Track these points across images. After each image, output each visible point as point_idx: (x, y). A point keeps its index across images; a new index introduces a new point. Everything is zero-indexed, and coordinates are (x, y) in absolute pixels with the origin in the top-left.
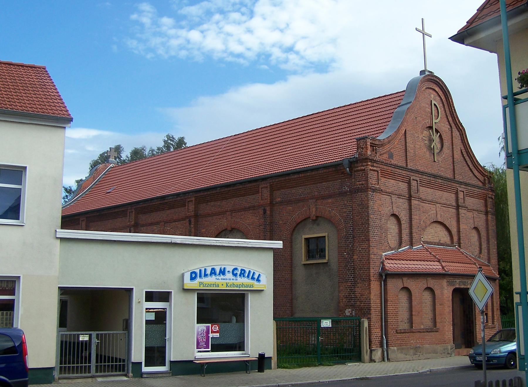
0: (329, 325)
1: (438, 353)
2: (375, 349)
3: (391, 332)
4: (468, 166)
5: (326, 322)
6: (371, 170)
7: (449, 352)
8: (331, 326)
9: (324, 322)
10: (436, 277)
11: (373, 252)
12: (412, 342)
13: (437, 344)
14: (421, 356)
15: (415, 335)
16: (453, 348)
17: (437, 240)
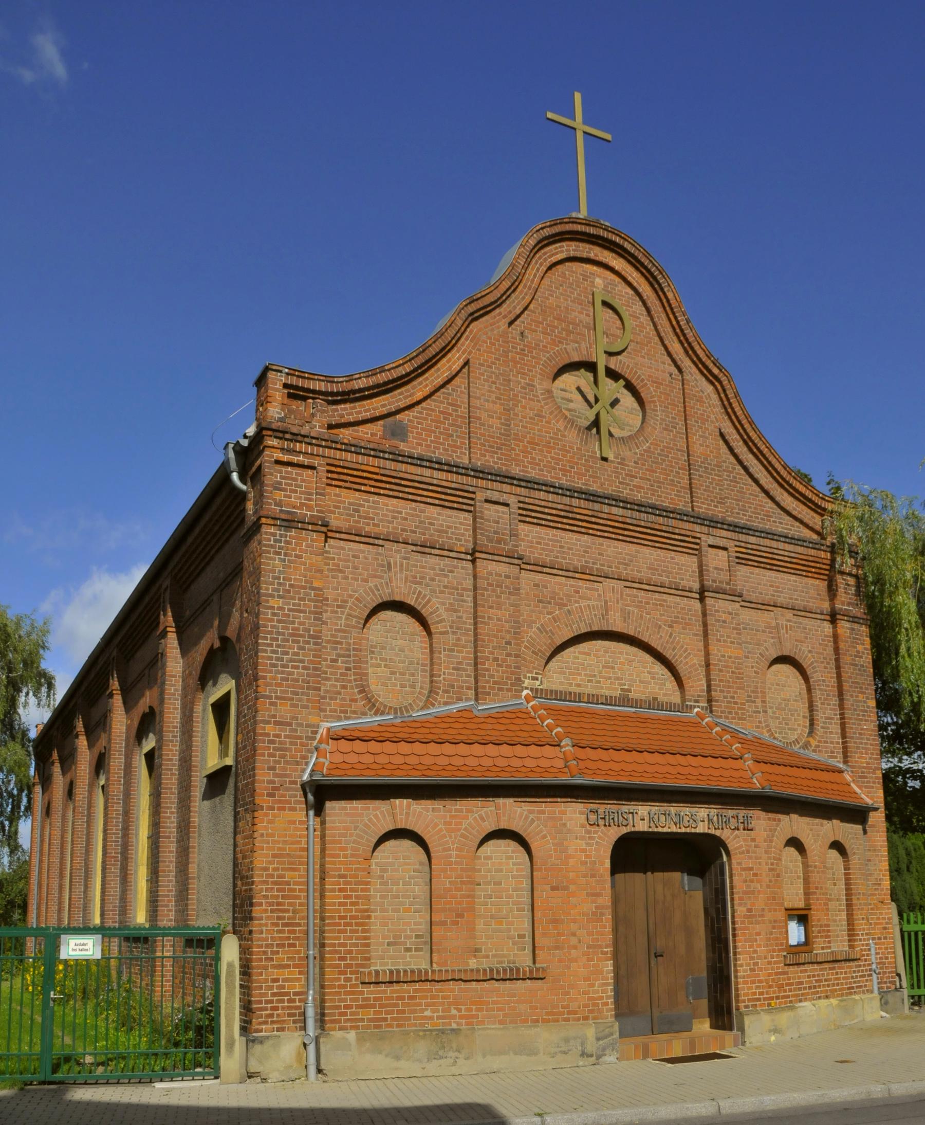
0: (91, 953)
1: (536, 1054)
2: (268, 1037)
3: (339, 979)
4: (756, 481)
5: (78, 941)
6: (278, 462)
7: (590, 1049)
12: (428, 1013)
13: (537, 1021)
14: (461, 1061)
15: (441, 991)
16: (612, 1034)
17: (616, 689)
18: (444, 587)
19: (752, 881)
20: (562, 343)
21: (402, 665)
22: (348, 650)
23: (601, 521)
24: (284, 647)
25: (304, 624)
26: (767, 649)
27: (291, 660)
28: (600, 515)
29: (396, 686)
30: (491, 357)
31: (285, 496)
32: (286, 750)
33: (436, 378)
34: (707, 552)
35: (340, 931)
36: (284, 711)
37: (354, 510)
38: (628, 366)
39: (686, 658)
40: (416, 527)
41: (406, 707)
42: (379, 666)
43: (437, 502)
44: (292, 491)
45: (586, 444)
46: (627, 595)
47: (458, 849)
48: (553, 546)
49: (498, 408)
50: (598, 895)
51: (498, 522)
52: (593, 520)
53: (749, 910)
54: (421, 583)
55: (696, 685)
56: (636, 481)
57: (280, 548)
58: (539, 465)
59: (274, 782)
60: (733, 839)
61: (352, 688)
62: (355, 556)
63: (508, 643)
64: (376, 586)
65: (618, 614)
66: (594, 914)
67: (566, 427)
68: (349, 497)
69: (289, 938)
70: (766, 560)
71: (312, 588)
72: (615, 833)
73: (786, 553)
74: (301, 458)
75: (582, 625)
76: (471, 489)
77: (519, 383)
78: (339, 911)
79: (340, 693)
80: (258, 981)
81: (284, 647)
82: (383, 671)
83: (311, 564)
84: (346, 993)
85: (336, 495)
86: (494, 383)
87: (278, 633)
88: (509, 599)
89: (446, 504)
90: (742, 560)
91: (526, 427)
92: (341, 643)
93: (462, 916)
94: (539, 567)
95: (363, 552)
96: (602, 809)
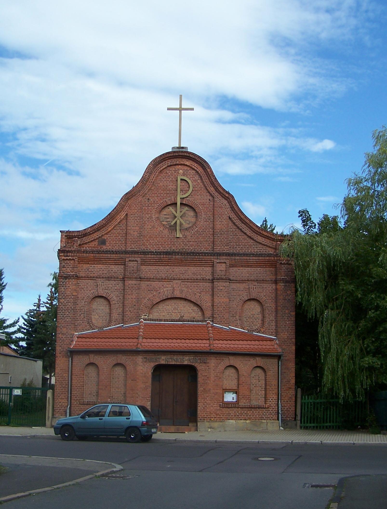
0: (19, 393)
2: (57, 417)
8: (21, 394)
9: (15, 391)
10: (149, 354)
11: (61, 332)
18: (115, 290)
19: (206, 380)
20: (164, 199)
21: (102, 314)
22: (85, 312)
23: (172, 261)
24: (64, 313)
25: (70, 306)
26: (243, 297)
27: (66, 316)
28: (172, 259)
29: (100, 320)
30: (135, 211)
31: (66, 269)
32: (65, 341)
33: (116, 222)
34: (216, 265)
35: (76, 390)
36: (64, 330)
37: (87, 270)
38: (191, 201)
39: (206, 303)
40: (107, 272)
41: (103, 327)
42: (95, 315)
43: (114, 263)
44: (68, 267)
45: (171, 233)
46: (183, 284)
47: (106, 369)
48: (155, 271)
49: (137, 228)
50: (147, 382)
51: (134, 267)
52: (169, 261)
53: (204, 389)
54: (108, 290)
55: (208, 313)
56: (191, 243)
57: (64, 285)
58: (152, 244)
59: (61, 350)
60: (200, 367)
61: (85, 322)
62: (87, 284)
63: (135, 305)
64: (93, 292)
65: (178, 292)
66: (145, 388)
67: (163, 229)
68: (85, 266)
69: (64, 391)
70: (245, 264)
71: (73, 295)
72: (153, 365)
73: (254, 260)
74: (70, 257)
75: (164, 296)
76: (124, 258)
77: (146, 217)
78: (75, 385)
79: (82, 324)
80: (56, 402)
81: (64, 313)
82: (97, 317)
83: (72, 288)
84: (77, 406)
85: (82, 266)
86: (136, 220)
87: (63, 309)
88: (136, 291)
89: (117, 263)
90: (232, 266)
91: (148, 232)
92: (82, 310)
93: (107, 387)
94: (149, 279)
95: (89, 282)
96: (148, 357)
